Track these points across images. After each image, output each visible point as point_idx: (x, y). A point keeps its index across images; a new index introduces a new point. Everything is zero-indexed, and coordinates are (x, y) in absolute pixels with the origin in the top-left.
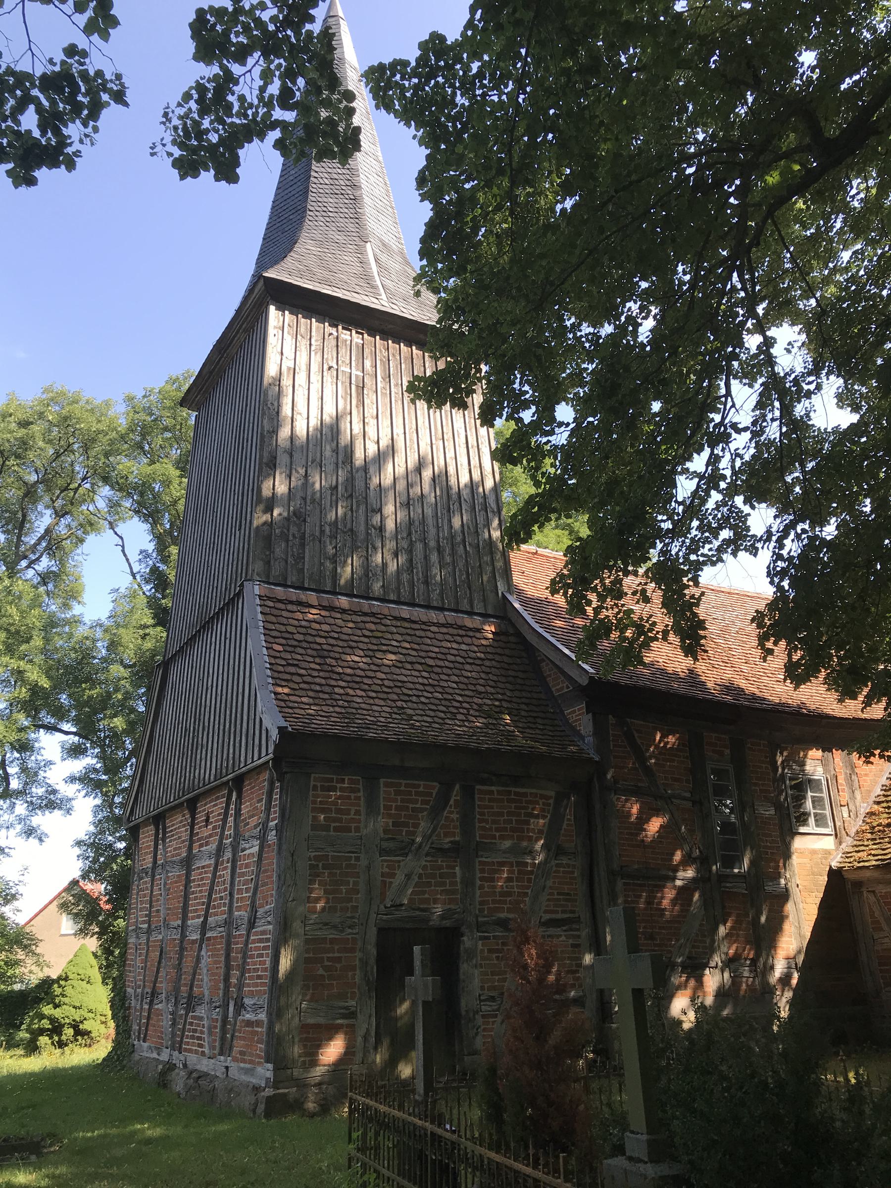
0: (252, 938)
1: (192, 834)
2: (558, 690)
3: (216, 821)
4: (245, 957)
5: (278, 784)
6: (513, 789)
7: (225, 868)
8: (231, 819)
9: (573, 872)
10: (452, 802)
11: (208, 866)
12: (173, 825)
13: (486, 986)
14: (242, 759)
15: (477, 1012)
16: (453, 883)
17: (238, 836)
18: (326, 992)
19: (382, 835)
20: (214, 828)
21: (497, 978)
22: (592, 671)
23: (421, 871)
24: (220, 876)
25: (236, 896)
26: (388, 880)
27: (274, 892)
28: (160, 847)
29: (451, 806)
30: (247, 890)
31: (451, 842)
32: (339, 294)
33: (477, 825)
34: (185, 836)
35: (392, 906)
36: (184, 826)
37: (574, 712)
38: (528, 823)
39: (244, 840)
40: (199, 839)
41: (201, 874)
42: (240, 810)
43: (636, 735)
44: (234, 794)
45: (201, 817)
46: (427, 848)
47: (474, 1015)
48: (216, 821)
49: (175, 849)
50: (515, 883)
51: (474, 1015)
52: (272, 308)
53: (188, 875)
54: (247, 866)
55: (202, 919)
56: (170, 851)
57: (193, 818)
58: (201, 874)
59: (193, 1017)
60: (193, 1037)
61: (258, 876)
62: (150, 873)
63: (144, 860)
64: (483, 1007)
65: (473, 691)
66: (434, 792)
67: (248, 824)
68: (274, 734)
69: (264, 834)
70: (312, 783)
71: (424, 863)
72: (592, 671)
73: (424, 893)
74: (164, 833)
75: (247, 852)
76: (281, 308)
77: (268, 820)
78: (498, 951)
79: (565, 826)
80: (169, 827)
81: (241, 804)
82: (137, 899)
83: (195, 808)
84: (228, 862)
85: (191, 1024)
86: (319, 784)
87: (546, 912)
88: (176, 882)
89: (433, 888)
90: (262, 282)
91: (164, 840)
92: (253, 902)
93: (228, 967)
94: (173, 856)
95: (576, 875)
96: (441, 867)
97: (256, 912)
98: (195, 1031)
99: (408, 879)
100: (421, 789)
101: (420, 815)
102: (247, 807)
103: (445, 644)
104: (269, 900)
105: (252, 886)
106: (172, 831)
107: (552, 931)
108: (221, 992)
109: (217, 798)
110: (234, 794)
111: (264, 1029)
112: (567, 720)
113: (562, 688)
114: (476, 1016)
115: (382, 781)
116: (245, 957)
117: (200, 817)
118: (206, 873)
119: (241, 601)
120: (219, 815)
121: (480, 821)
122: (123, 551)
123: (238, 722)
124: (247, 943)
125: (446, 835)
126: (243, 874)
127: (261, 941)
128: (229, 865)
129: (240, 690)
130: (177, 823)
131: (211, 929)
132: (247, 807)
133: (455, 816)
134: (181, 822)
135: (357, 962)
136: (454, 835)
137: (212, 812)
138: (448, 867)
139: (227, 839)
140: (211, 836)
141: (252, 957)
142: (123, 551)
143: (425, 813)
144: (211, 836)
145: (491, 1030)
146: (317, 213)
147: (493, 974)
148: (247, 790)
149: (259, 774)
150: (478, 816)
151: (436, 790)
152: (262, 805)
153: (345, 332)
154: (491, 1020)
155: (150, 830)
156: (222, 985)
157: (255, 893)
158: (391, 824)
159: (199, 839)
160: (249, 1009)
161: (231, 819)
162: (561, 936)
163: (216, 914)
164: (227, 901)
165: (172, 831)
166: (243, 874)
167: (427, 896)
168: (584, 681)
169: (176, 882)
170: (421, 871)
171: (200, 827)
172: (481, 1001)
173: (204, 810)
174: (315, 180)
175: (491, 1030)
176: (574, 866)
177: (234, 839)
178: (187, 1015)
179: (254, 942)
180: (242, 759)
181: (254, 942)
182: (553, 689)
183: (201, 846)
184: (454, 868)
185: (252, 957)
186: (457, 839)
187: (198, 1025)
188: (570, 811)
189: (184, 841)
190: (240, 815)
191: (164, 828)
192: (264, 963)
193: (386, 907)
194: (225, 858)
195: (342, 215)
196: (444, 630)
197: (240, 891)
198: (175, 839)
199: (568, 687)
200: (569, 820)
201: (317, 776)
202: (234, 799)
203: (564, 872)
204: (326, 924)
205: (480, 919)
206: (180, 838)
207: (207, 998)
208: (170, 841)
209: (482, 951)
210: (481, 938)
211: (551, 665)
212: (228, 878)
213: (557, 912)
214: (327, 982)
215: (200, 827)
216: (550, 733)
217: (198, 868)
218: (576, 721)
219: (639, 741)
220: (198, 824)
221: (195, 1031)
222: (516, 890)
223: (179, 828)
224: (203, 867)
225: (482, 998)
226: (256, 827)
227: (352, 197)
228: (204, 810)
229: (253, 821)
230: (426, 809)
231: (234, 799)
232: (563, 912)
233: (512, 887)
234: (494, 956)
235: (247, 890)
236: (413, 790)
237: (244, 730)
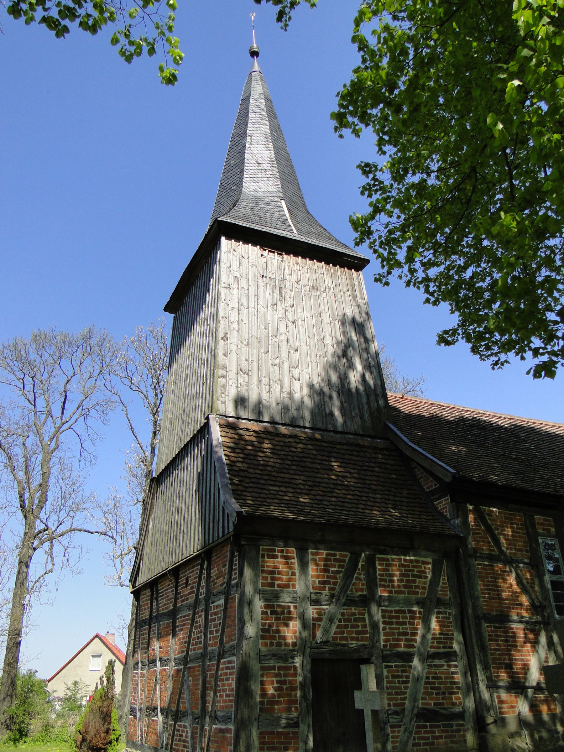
0: (221, 666)
1: (176, 594)
2: (428, 488)
3: (193, 583)
4: (216, 680)
5: (236, 554)
6: (403, 557)
7: (200, 616)
8: (204, 581)
9: (449, 618)
10: (360, 566)
11: (188, 615)
12: (163, 588)
13: (392, 703)
14: (211, 538)
15: (386, 724)
16: (365, 626)
17: (209, 593)
18: (276, 707)
19: (312, 590)
20: (192, 588)
21: (399, 697)
22: (452, 471)
23: (340, 617)
24: (197, 622)
25: (209, 636)
26: (317, 623)
27: (236, 632)
28: (155, 604)
29: (359, 570)
30: (217, 631)
31: (360, 595)
32: (266, 229)
33: (379, 583)
34: (172, 595)
35: (321, 642)
36: (171, 588)
37: (442, 502)
38: (414, 581)
39: (213, 595)
40: (182, 597)
41: (183, 621)
42: (210, 574)
43: (487, 517)
44: (206, 563)
45: (182, 581)
46: (344, 600)
47: (384, 726)
48: (193, 583)
49: (165, 605)
50: (408, 626)
51: (384, 726)
52: (223, 239)
53: (174, 623)
54: (216, 613)
55: (184, 654)
56: (162, 606)
57: (177, 582)
58: (183, 621)
59: (180, 726)
60: (179, 740)
61: (224, 620)
62: (147, 623)
63: (144, 613)
64: (391, 720)
65: (369, 489)
66: (347, 559)
67: (216, 583)
68: (233, 518)
69: (228, 590)
70: (261, 552)
71: (343, 611)
72: (452, 471)
73: (343, 632)
74: (157, 594)
75: (216, 604)
76: (229, 238)
77: (230, 579)
78: (398, 677)
79: (441, 584)
80: (160, 590)
81: (210, 569)
82: (139, 642)
83: (179, 575)
84: (202, 611)
85: (178, 730)
86: (266, 553)
87: (431, 647)
88: (166, 628)
89: (349, 629)
90: (216, 222)
91: (157, 598)
92: (221, 640)
93: (204, 689)
94: (163, 609)
95: (451, 620)
96: (354, 614)
97: (224, 647)
98: (181, 736)
99: (331, 623)
100: (338, 557)
101: (338, 576)
102: (215, 571)
103: (347, 457)
104: (233, 638)
105: (220, 628)
106: (162, 593)
107: (437, 662)
108: (199, 707)
109: (193, 567)
110: (206, 563)
111: (232, 735)
112: (436, 508)
113: (431, 486)
114: (386, 726)
115: (310, 551)
116: (216, 680)
117: (182, 581)
118: (187, 620)
119: (207, 430)
120: (196, 578)
121: (381, 580)
122: (127, 415)
123: (207, 512)
124: (217, 670)
125: (357, 590)
126: (213, 620)
127: (227, 668)
128: (203, 613)
129: (208, 490)
130: (166, 587)
131: (191, 661)
132: (215, 571)
133: (362, 577)
134: (169, 585)
135: (298, 684)
136: (362, 590)
137: (190, 577)
138: (359, 614)
139: (201, 595)
140: (190, 594)
141: (222, 680)
142: (127, 415)
143: (341, 575)
144: (190, 594)
145: (398, 737)
146: (250, 184)
147: (396, 694)
148: (215, 559)
149: (223, 547)
150: (379, 577)
151: (349, 557)
152: (226, 570)
153: (270, 253)
154: (397, 729)
155: (148, 593)
156: (200, 702)
157: (222, 634)
158: (317, 582)
159: (182, 597)
160: (220, 719)
161: (204, 581)
162: (443, 665)
163: (194, 650)
164: (202, 640)
165: (162, 593)
166: (213, 620)
167: (345, 635)
168: (448, 479)
169: (166, 628)
170: (340, 617)
171: (182, 588)
172: (388, 715)
173: (185, 576)
174: (248, 161)
175: (398, 737)
176: (449, 613)
177: (207, 594)
178: (175, 724)
179: (222, 669)
180: (211, 538)
181: (222, 669)
182: (425, 487)
183: (183, 601)
184: (363, 614)
185: (222, 680)
186: (365, 593)
187: (183, 731)
188: (444, 573)
189: (170, 599)
190: (210, 577)
191: (157, 591)
192: (231, 685)
193: (317, 643)
194: (200, 609)
195: (265, 184)
196: (345, 447)
197: (211, 632)
198: (164, 598)
199: (435, 485)
200: (443, 579)
201: (264, 547)
202: (205, 566)
203: (442, 618)
204: (274, 655)
205: (385, 652)
206: (168, 596)
207: (189, 712)
208: (161, 599)
209: (387, 677)
210: (386, 667)
211: (422, 470)
212: (203, 623)
213: (439, 648)
214: (430, 690)
215: (182, 588)
216: (426, 517)
217: (181, 617)
218: (444, 509)
219: (489, 522)
220: (181, 585)
221: (181, 736)
222: (408, 631)
223: (167, 589)
224: (185, 616)
225: (389, 712)
226: (222, 585)
227: (271, 173)
228: (185, 576)
229: (220, 581)
230: (341, 572)
231: (205, 566)
232: (444, 647)
233: (406, 629)
234: (396, 680)
235: (217, 631)
236: (332, 558)
237: (211, 518)
